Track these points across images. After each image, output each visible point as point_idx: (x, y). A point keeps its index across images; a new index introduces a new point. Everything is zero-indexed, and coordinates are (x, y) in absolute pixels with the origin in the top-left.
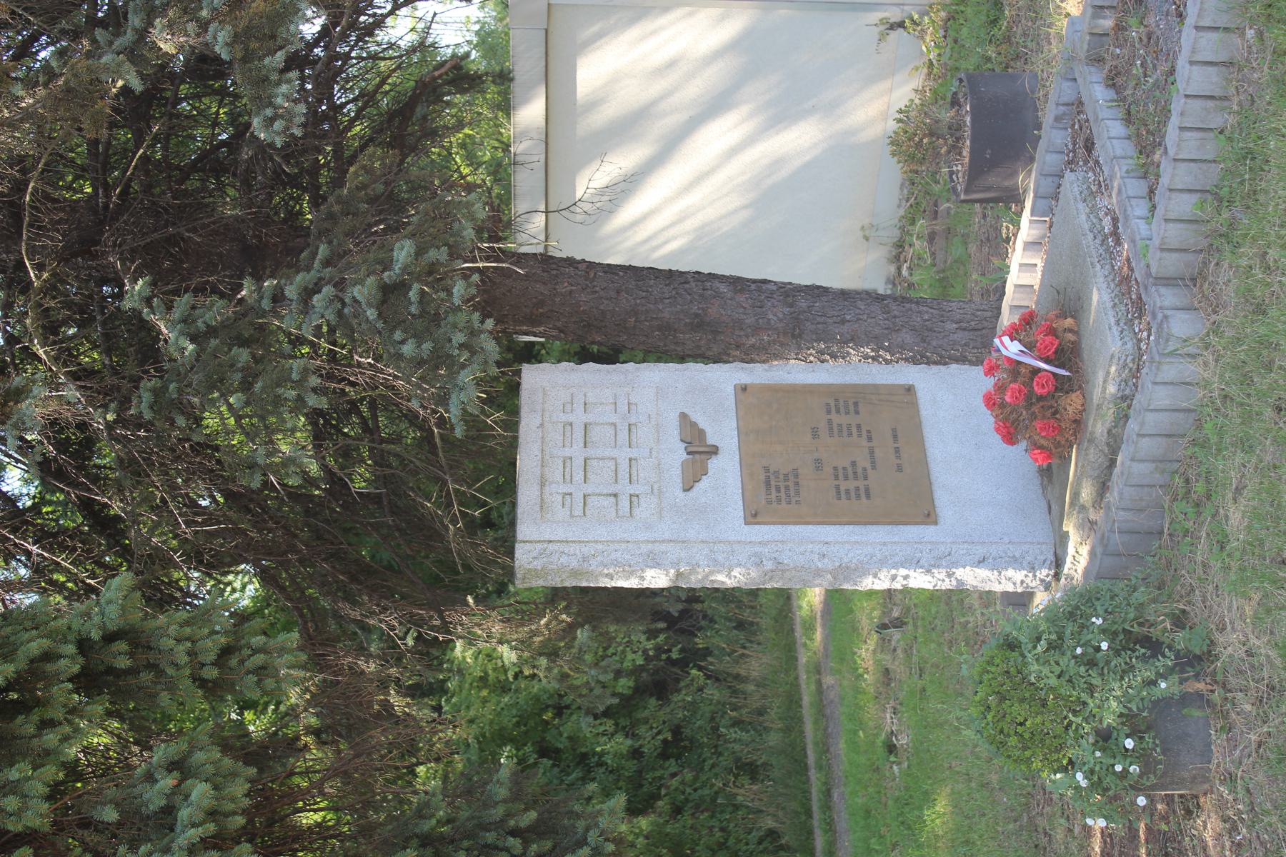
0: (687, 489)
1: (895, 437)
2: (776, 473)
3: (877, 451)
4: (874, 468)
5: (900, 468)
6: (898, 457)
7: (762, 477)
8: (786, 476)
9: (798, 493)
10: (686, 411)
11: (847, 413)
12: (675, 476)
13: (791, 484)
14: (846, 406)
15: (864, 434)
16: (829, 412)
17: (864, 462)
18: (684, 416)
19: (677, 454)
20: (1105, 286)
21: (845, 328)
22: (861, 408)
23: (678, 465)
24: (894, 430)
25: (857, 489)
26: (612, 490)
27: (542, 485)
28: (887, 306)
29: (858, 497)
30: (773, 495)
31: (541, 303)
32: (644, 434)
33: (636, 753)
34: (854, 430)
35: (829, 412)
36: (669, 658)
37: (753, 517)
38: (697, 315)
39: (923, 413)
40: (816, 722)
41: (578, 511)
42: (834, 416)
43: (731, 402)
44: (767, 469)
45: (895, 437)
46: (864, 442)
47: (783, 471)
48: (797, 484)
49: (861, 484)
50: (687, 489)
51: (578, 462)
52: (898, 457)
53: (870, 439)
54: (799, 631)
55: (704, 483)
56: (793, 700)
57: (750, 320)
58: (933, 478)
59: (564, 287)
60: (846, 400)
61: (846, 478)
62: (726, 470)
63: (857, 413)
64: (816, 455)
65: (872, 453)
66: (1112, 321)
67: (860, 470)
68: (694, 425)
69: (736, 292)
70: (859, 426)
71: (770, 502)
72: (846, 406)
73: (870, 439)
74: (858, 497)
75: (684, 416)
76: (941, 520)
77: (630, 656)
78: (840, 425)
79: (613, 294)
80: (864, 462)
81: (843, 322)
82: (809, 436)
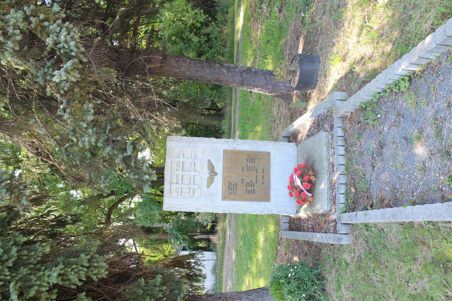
0: (208, 187)
1: (263, 171)
2: (231, 184)
3: (258, 176)
4: (256, 183)
5: (263, 184)
6: (263, 179)
7: (228, 185)
8: (234, 185)
9: (236, 192)
10: (210, 159)
11: (252, 162)
12: (205, 182)
13: (235, 188)
14: (252, 160)
15: (255, 170)
16: (247, 162)
17: (254, 181)
18: (209, 161)
19: (206, 174)
20: (326, 183)
21: (255, 83)
22: (256, 161)
23: (206, 179)
24: (263, 169)
25: (251, 190)
26: (184, 173)
27: (171, 184)
28: (266, 77)
29: (251, 193)
30: (231, 191)
31: (176, 73)
32: (198, 167)
33: (200, 42)
34: (253, 169)
35: (247, 162)
36: (208, 20)
37: (224, 198)
38: (217, 79)
39: (271, 162)
40: (237, 54)
41: (180, 195)
42: (248, 163)
43: (222, 156)
44: (229, 182)
45: (263, 171)
46: (255, 173)
47: (233, 183)
48: (236, 188)
49: (252, 188)
50: (208, 187)
51: (180, 176)
52: (263, 179)
53: (257, 172)
54: (236, 32)
55: (212, 186)
56: (233, 43)
57: (230, 80)
58: (271, 185)
59: (182, 69)
60: (253, 157)
61: (249, 186)
62: (219, 180)
63: (254, 162)
64: (242, 178)
65: (256, 177)
66: (326, 198)
67: (253, 184)
68: (212, 164)
69: (228, 72)
70: (254, 167)
71: (229, 194)
72: (252, 160)
73: (257, 172)
74: (251, 193)
75: (209, 161)
76: (271, 201)
77: (200, 19)
78: (249, 167)
79: (195, 72)
80: (254, 181)
81: (254, 82)
82: (241, 171)
